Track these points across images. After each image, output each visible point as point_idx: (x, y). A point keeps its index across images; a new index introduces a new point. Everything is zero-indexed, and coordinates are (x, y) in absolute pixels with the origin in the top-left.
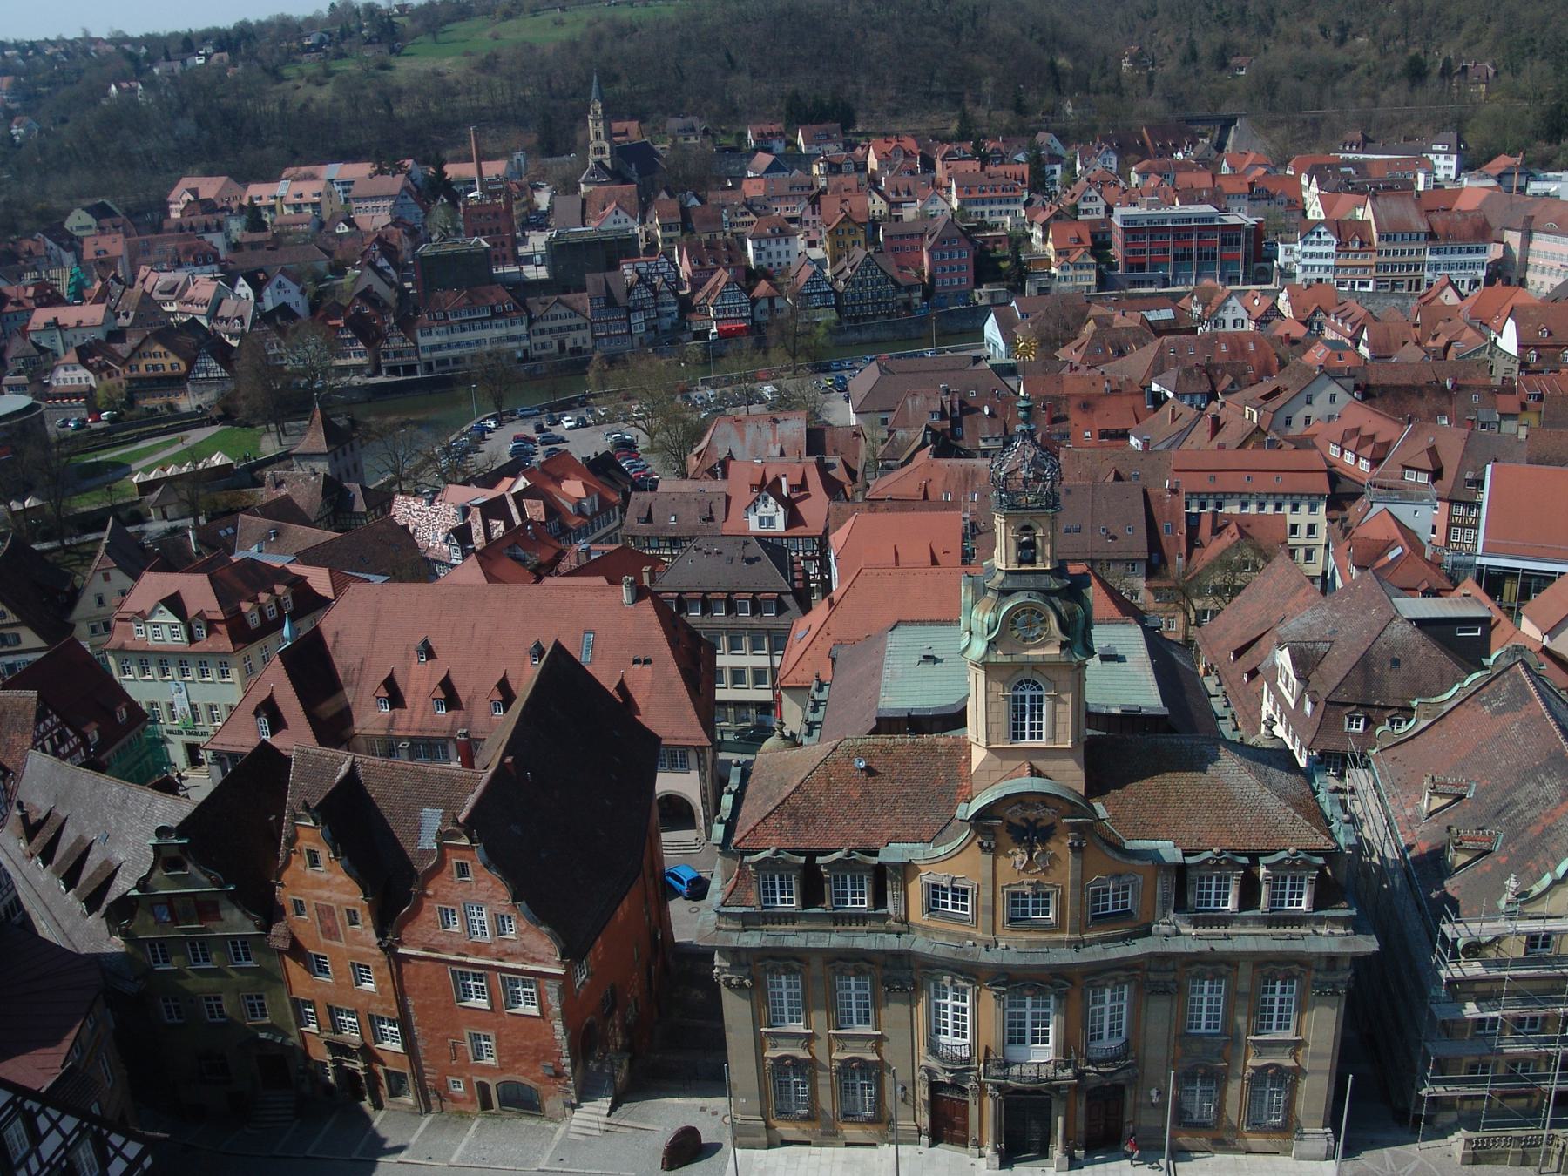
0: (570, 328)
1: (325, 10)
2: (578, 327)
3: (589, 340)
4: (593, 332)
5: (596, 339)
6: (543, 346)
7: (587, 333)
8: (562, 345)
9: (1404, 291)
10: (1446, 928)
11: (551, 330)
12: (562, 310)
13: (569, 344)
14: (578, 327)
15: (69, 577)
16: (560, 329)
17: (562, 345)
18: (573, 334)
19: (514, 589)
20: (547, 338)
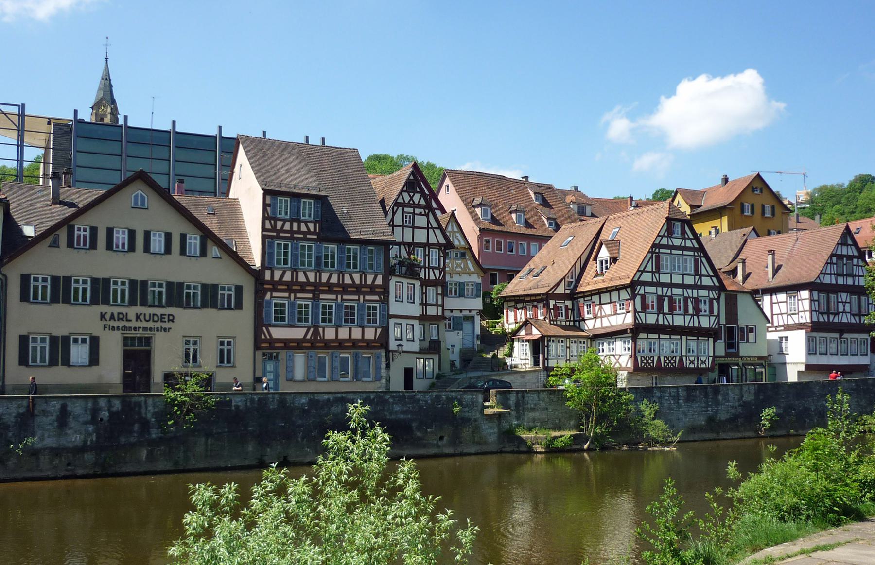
0: (177, 294)
1: (847, 184)
2: (210, 297)
3: (244, 350)
4: (260, 323)
5: (265, 346)
6: (59, 350)
7: (238, 324)
8: (137, 359)
9: (758, 193)
10: (792, 377)
11: (101, 290)
12: (160, 220)
13: (165, 358)
14: (210, 297)
15: (16, 422)
16: (139, 291)
17: (137, 359)
18: (188, 321)
19: (764, 238)
20: (80, 319)
